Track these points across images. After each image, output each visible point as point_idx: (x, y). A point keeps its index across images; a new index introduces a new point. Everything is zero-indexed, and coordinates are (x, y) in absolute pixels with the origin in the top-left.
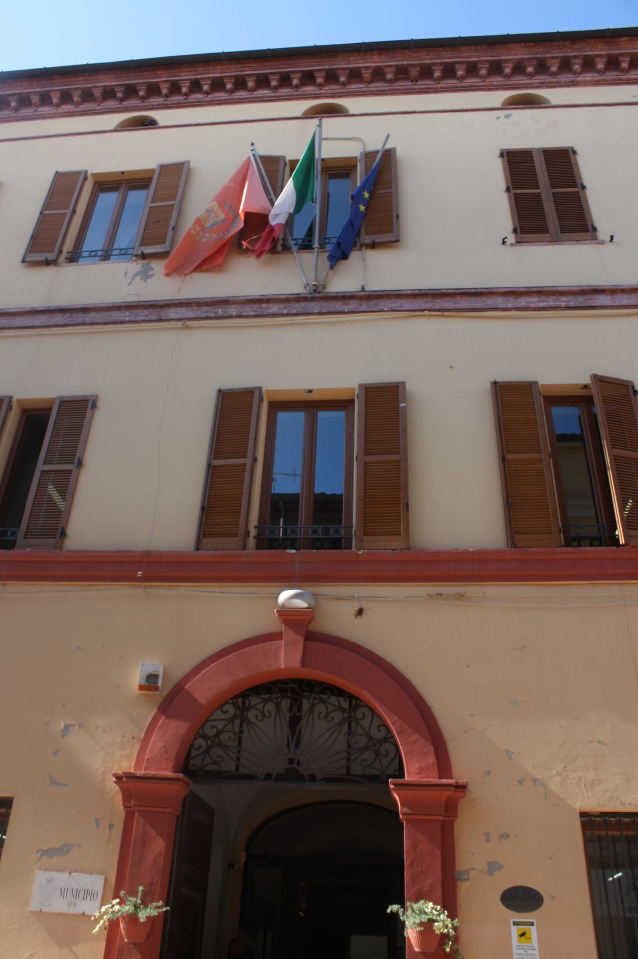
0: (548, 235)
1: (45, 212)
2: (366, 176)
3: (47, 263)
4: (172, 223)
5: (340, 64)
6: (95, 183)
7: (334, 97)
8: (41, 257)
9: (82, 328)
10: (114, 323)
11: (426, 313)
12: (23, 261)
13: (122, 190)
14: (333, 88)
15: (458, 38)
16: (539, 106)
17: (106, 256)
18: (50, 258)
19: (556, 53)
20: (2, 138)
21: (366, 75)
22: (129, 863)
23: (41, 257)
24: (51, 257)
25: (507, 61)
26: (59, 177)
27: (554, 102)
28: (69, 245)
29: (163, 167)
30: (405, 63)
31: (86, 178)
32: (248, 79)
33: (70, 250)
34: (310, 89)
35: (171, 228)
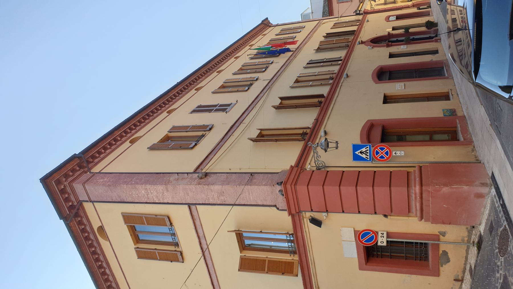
1: (159, 259)
2: (157, 143)
3: (181, 254)
4: (154, 216)
5: (171, 95)
6: (137, 243)
7: (216, 70)
8: (180, 257)
12: (183, 262)
13: (137, 233)
17: (174, 234)
18: (180, 254)
20: (129, 288)
22: (414, 206)
23: (180, 257)
24: (179, 254)
26: (139, 257)
28: (172, 248)
29: (126, 223)
31: (138, 248)
33: (174, 247)
35: (156, 217)
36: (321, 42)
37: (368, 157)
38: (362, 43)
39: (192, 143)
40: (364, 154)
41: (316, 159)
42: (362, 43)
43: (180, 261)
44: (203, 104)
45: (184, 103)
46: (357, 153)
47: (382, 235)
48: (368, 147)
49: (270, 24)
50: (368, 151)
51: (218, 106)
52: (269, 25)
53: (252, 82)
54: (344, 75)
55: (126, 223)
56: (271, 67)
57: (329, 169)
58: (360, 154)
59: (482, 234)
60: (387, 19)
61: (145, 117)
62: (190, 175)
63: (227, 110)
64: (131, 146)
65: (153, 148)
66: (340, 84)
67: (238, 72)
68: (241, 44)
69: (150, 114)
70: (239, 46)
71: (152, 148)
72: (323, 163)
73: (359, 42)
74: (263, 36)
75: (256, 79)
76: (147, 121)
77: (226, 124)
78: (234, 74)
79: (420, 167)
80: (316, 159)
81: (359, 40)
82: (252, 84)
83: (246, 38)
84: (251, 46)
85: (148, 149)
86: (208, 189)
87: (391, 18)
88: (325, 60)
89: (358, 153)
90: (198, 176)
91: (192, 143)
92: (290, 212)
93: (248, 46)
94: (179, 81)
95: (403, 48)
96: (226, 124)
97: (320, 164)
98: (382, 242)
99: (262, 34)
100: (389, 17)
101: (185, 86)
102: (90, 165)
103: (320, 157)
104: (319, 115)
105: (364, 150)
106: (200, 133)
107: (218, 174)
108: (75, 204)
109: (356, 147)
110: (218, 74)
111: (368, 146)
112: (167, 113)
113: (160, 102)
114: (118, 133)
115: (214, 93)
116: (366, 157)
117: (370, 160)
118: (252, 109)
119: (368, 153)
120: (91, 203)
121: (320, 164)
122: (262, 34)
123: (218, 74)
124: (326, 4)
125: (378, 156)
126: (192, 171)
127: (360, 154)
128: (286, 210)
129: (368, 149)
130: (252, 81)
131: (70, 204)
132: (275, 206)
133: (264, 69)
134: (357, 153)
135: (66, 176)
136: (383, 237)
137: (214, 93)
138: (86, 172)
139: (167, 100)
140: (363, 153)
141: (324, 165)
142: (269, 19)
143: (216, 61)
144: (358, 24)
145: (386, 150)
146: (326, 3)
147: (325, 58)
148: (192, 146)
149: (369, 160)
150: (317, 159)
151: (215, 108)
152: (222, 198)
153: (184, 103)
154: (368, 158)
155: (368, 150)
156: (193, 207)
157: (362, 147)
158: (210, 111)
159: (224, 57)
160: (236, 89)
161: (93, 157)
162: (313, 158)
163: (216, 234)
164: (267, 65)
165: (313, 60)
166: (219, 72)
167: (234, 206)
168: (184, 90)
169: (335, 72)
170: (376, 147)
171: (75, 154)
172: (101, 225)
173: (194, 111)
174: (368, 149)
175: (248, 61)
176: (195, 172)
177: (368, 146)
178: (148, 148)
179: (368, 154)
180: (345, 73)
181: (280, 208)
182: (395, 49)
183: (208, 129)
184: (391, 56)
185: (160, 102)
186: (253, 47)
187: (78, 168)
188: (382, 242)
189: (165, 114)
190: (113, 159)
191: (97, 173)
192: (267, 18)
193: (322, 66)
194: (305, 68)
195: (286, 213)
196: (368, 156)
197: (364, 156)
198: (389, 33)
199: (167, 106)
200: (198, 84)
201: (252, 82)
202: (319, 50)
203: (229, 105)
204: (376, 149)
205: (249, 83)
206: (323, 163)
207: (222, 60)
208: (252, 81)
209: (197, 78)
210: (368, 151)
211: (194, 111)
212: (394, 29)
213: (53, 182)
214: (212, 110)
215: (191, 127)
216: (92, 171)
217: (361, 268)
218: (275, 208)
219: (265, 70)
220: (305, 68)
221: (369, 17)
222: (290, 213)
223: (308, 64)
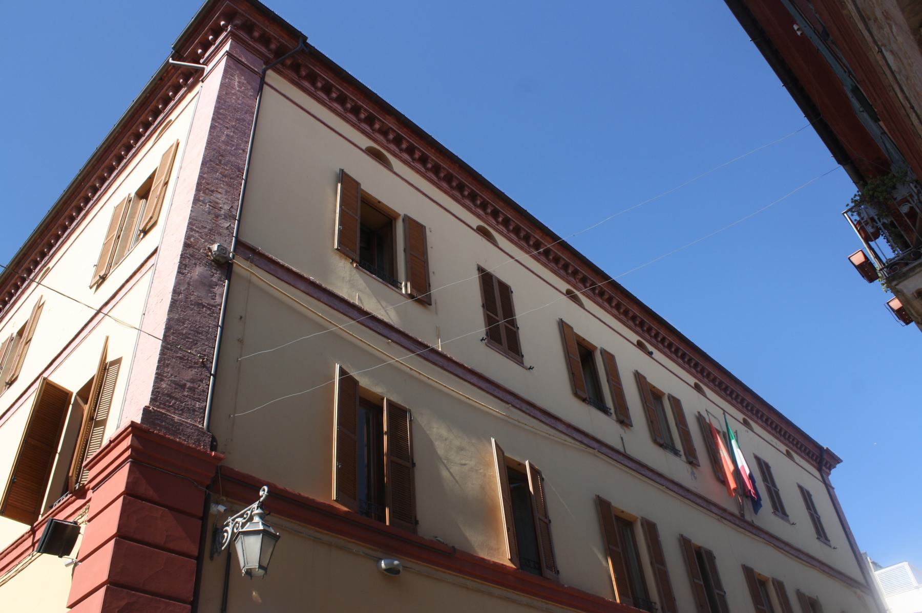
0: (501, 347)
7: (748, 418)
9: (685, 500)
10: (697, 504)
11: (772, 545)
14: (393, 147)
15: (524, 210)
16: (384, 164)
19: (584, 272)
21: (417, 155)
25: (747, 400)
27: (395, 170)
30: (638, 314)
32: (404, 142)
34: (380, 137)
39: (823, 535)
45: (713, 402)
49: (828, 471)
51: (775, 489)
52: (824, 468)
61: (588, 281)
63: (777, 512)
65: (564, 328)
69: (498, 217)
77: (622, 438)
82: (677, 456)
85: (697, 414)
91: (823, 535)
92: (6, 552)
96: (622, 438)
99: (790, 450)
106: (679, 445)
110: (784, 454)
118: (501, 400)
122: (790, 450)
123: (739, 422)
142: (838, 466)
148: (580, 393)
153: (713, 402)
158: (808, 508)
161: (312, 78)
166: (788, 455)
168: (560, 266)
183: (691, 459)
189: (635, 338)
192: (838, 461)
200: (395, 155)
202: (685, 543)
203: (826, 538)
209: (807, 451)
213: (227, 2)
214: (810, 509)
216: (270, 73)
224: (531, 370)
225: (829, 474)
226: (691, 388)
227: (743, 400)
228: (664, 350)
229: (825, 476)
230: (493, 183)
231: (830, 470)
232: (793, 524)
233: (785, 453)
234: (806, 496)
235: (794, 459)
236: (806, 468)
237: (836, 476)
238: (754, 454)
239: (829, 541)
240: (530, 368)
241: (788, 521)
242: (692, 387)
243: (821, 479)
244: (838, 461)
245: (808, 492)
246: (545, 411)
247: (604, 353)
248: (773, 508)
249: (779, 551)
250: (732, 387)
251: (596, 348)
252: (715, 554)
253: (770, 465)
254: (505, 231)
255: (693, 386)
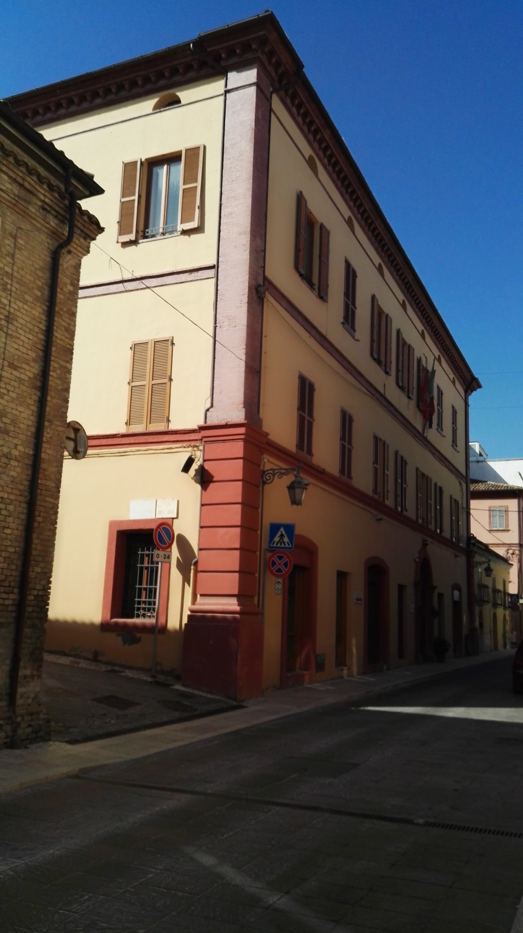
27: (385, 278)
36: (431, 480)
37: (275, 545)
38: (425, 545)
40: (280, 540)
41: (276, 471)
42: (425, 545)
43: (120, 237)
44: (358, 280)
46: (282, 530)
47: (167, 556)
48: (289, 545)
50: (283, 545)
53: (383, 364)
54: (380, 516)
55: (186, 150)
56: (403, 397)
57: (261, 488)
58: (279, 534)
59: (172, 687)
60: (457, 587)
62: (261, 272)
63: (346, 325)
64: (418, 333)
66: (368, 508)
67: (303, 214)
68: (444, 342)
70: (441, 338)
71: (300, 199)
72: (270, 481)
73: (427, 540)
74: (452, 380)
75: (387, 371)
76: (347, 197)
77: (385, 385)
78: (398, 332)
79: (257, 614)
80: (276, 471)
81: (429, 540)
83: (453, 350)
84: (439, 360)
85: (419, 358)
86: (241, 302)
87: (456, 593)
88: (404, 485)
89: (281, 532)
90: (260, 285)
91: (440, 427)
93: (423, 328)
94: (440, 312)
95: (410, 606)
96: (385, 385)
97: (269, 476)
98: (158, 556)
99: (425, 330)
100: (460, 590)
101: (332, 150)
102: (282, 93)
103: (279, 477)
104: (330, 476)
105: (286, 539)
107: (261, 317)
108: (223, 63)
109: (289, 529)
111: (291, 546)
112: (350, 218)
113: (367, 206)
114: (327, 134)
115: (373, 298)
116: (274, 542)
117: (270, 547)
119: (281, 544)
120: (222, 92)
121: (269, 476)
123: (419, 332)
124: (491, 487)
125: (275, 558)
126: (267, 274)
127: (279, 534)
128: (206, 422)
129: (287, 546)
130: (386, 365)
131: (223, 55)
132: (212, 406)
133: (401, 384)
134: (282, 530)
135: (271, 54)
136: (165, 558)
137: (373, 298)
138: (272, 85)
139: (369, 217)
140: (282, 538)
141: (268, 482)
142: (479, 390)
143: (422, 299)
144: (454, 539)
145: (285, 570)
146: (493, 487)
147: (407, 486)
149: (271, 545)
150: (278, 473)
151: (350, 303)
152: (226, 324)
154: (273, 544)
155: (285, 545)
156: (212, 272)
157: (290, 537)
158: (453, 423)
159: (427, 313)
160: (375, 338)
162: (277, 468)
163: (176, 309)
164: (406, 390)
165: (407, 466)
166: (380, 269)
167: (212, 338)
169: (386, 501)
170: (288, 557)
171: (303, 66)
172: (183, 102)
173: (453, 407)
174: (287, 546)
175: (395, 326)
176: (265, 278)
177: (291, 546)
178: (301, 192)
179: (279, 545)
180: (384, 517)
181: (208, 412)
182: (410, 594)
184: (401, 588)
185: (367, 206)
186: (437, 363)
187: (280, 71)
188: (158, 556)
190: (301, 149)
191: (271, 106)
193: (396, 481)
194: (396, 453)
195: (201, 423)
196: (277, 544)
197: (277, 539)
198: (435, 588)
199: (360, 217)
201: (383, 364)
204: (285, 557)
205: (383, 359)
206: (270, 481)
207: (342, 176)
208: (386, 365)
209: (398, 267)
210: (283, 545)
211: (453, 407)
212: (441, 595)
215: (413, 372)
217: (112, 524)
218: (208, 405)
219: (374, 359)
220: (396, 453)
221: (462, 560)
222: (202, 428)
223: (402, 457)
224: (357, 341)
225: (470, 394)
226: (343, 220)
227: (353, 192)
228: (349, 203)
229: (467, 395)
230: (361, 171)
231: (472, 392)
232: (357, 340)
233: (377, 265)
234: (454, 412)
235: (425, 339)
236: (389, 285)
237: (473, 398)
238: (346, 257)
239: (355, 331)
240: (444, 436)
241: (353, 337)
242: (345, 220)
243: (464, 398)
244: (480, 386)
245: (442, 392)
246: (355, 368)
247: (322, 226)
248: (344, 318)
249: (440, 463)
250: (355, 186)
251: (317, 221)
252: (316, 387)
253: (358, 274)
254: (336, 178)
255: (347, 219)
